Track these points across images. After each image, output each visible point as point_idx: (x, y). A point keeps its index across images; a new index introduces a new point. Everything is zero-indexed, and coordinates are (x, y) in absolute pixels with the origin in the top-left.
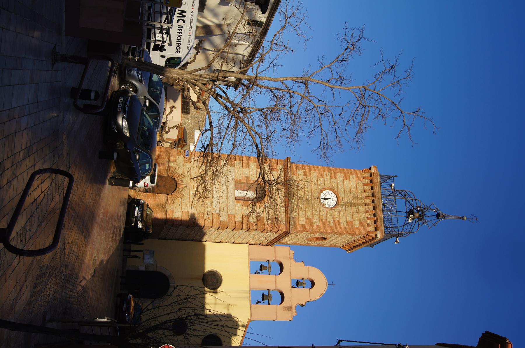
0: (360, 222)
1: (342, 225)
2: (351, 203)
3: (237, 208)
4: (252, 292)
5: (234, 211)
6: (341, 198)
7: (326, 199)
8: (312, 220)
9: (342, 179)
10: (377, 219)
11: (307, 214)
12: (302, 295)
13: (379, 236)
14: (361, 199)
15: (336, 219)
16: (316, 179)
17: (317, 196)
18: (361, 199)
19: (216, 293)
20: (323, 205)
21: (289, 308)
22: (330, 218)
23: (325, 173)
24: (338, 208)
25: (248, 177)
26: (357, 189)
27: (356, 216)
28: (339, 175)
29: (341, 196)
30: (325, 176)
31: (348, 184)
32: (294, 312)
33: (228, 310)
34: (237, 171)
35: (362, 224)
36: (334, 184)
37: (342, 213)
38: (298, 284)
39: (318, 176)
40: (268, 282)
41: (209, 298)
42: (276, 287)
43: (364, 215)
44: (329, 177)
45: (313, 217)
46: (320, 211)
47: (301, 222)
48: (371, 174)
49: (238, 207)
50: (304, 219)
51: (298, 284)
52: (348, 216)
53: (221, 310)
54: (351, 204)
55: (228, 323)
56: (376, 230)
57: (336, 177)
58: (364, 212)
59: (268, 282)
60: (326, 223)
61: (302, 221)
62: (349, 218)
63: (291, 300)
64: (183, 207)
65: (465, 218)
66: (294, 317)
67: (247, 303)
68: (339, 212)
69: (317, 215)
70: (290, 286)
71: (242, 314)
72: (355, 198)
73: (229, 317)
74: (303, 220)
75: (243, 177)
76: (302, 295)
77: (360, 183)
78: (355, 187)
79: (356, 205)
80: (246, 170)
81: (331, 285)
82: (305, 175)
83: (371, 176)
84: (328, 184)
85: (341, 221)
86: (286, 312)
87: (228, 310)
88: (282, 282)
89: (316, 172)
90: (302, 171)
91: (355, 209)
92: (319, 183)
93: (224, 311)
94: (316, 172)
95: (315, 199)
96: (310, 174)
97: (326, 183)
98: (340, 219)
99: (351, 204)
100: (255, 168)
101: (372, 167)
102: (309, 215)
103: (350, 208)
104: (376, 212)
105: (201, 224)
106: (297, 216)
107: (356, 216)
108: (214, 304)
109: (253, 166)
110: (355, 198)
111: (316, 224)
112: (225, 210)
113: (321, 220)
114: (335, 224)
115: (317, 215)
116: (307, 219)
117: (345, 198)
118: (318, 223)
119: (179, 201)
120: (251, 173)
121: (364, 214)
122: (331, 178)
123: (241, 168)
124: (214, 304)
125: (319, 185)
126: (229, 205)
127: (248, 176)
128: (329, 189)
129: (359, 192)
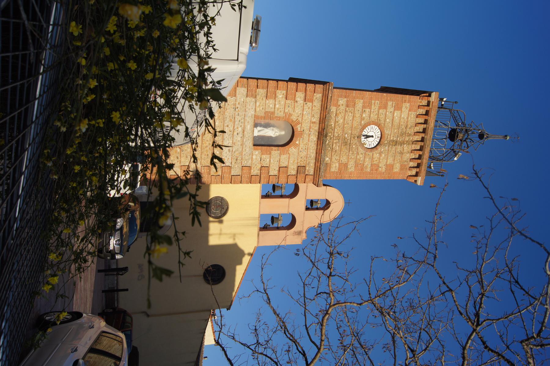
0: (401, 165)
1: (380, 169)
2: (396, 142)
3: (254, 157)
4: (262, 217)
5: (250, 161)
6: (386, 136)
7: (367, 137)
8: (346, 165)
9: (392, 110)
10: (422, 162)
11: (341, 159)
12: (314, 218)
13: (419, 183)
14: (409, 135)
15: (375, 163)
16: (360, 110)
17: (357, 134)
18: (409, 135)
19: (221, 222)
20: (363, 145)
21: (299, 233)
22: (368, 163)
23: (373, 102)
24: (379, 149)
25: (273, 113)
26: (407, 122)
27: (399, 158)
28: (390, 103)
29: (387, 132)
30: (373, 106)
31: (399, 116)
32: (304, 236)
33: (234, 239)
34: (258, 104)
35: (402, 168)
36: (382, 117)
37: (383, 155)
38: (311, 205)
39: (364, 107)
40: (279, 207)
41: (214, 227)
42: (288, 211)
43: (408, 156)
44: (377, 108)
45: (348, 161)
46: (358, 153)
47: (333, 170)
48: (429, 103)
49: (256, 155)
50: (337, 165)
51: (311, 205)
52: (389, 158)
53: (226, 240)
54: (396, 143)
55: (234, 253)
56: (417, 175)
57: (385, 107)
58: (408, 152)
59: (279, 207)
60: (362, 169)
61: (335, 168)
62: (390, 161)
63: (303, 225)
64: (183, 160)
65: (508, 138)
66: (304, 241)
67: (256, 229)
68: (380, 153)
69: (353, 159)
70: (304, 208)
71: (249, 241)
72: (402, 135)
73: (235, 247)
74: (336, 167)
75: (266, 112)
76: (314, 218)
77: (413, 114)
78: (406, 120)
79: (402, 143)
80: (270, 102)
81: (347, 203)
82: (347, 106)
83: (428, 105)
84: (374, 117)
85: (380, 165)
86: (296, 236)
87: (234, 239)
88: (296, 206)
89: (362, 101)
90: (346, 99)
91: (399, 148)
92: (364, 115)
93: (229, 241)
94: (362, 101)
95: (354, 138)
96: (355, 103)
97: (372, 115)
98: (380, 162)
99: (396, 143)
100: (284, 99)
101: (433, 95)
102: (344, 159)
103: (394, 148)
104: (424, 154)
105: (206, 182)
106: (329, 162)
107: (398, 157)
108: (218, 234)
109: (281, 96)
110: (402, 135)
111: (350, 170)
112: (239, 161)
113: (356, 165)
114: (372, 170)
115: (353, 159)
116: (340, 165)
117: (390, 134)
118: (353, 169)
119: (176, 152)
120: (277, 106)
121: (408, 155)
122: (380, 108)
123: (264, 99)
124: (218, 234)
125: (363, 119)
126: (244, 153)
127: (272, 110)
128: (379, 126)
129: (409, 126)
